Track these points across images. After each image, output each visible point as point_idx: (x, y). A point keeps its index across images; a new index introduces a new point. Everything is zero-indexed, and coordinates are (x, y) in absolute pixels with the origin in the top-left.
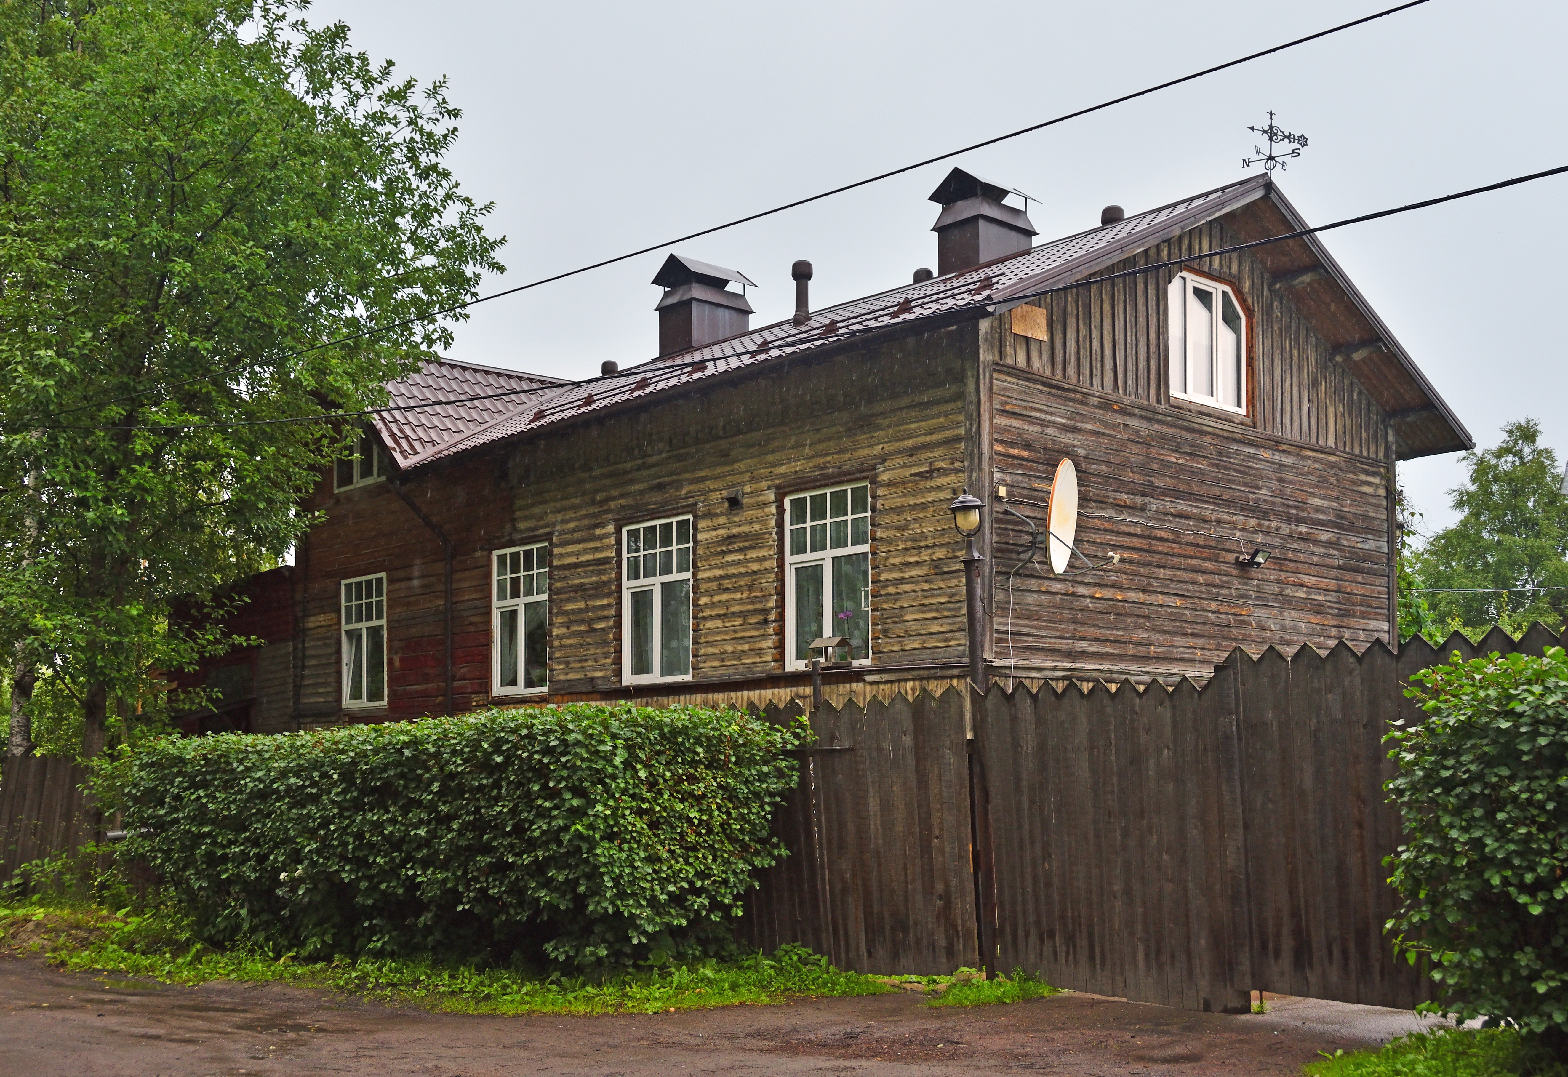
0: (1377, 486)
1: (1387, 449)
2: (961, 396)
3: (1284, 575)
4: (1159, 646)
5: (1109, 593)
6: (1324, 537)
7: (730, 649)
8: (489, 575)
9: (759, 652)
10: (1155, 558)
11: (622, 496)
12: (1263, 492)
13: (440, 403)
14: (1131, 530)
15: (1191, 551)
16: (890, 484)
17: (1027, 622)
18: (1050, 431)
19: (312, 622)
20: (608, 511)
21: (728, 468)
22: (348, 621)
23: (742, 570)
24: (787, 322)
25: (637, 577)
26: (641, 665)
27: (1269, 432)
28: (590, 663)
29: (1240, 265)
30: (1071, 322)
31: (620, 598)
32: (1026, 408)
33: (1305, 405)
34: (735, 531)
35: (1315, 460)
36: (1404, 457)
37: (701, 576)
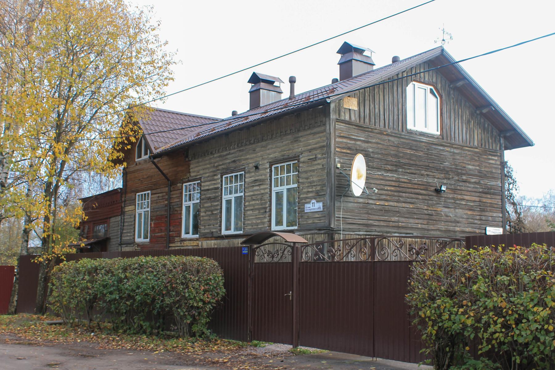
0: (496, 160)
1: (500, 146)
2: (325, 131)
3: (455, 196)
4: (403, 223)
5: (382, 203)
6: (473, 180)
7: (254, 222)
8: (182, 193)
9: (263, 223)
10: (401, 189)
11: (223, 164)
12: (446, 164)
13: (161, 132)
14: (391, 179)
15: (416, 186)
16: (303, 162)
17: (349, 214)
18: (358, 143)
19: (127, 209)
20: (218, 170)
21: (255, 155)
22: (186, 201)
23: (259, 193)
24: (287, 99)
25: (237, 193)
26: (228, 228)
27: (449, 141)
28: (212, 226)
29: (436, 79)
30: (367, 103)
31: (222, 202)
32: (349, 135)
33: (464, 129)
34: (257, 178)
35: (469, 151)
36: (506, 149)
37: (246, 194)
